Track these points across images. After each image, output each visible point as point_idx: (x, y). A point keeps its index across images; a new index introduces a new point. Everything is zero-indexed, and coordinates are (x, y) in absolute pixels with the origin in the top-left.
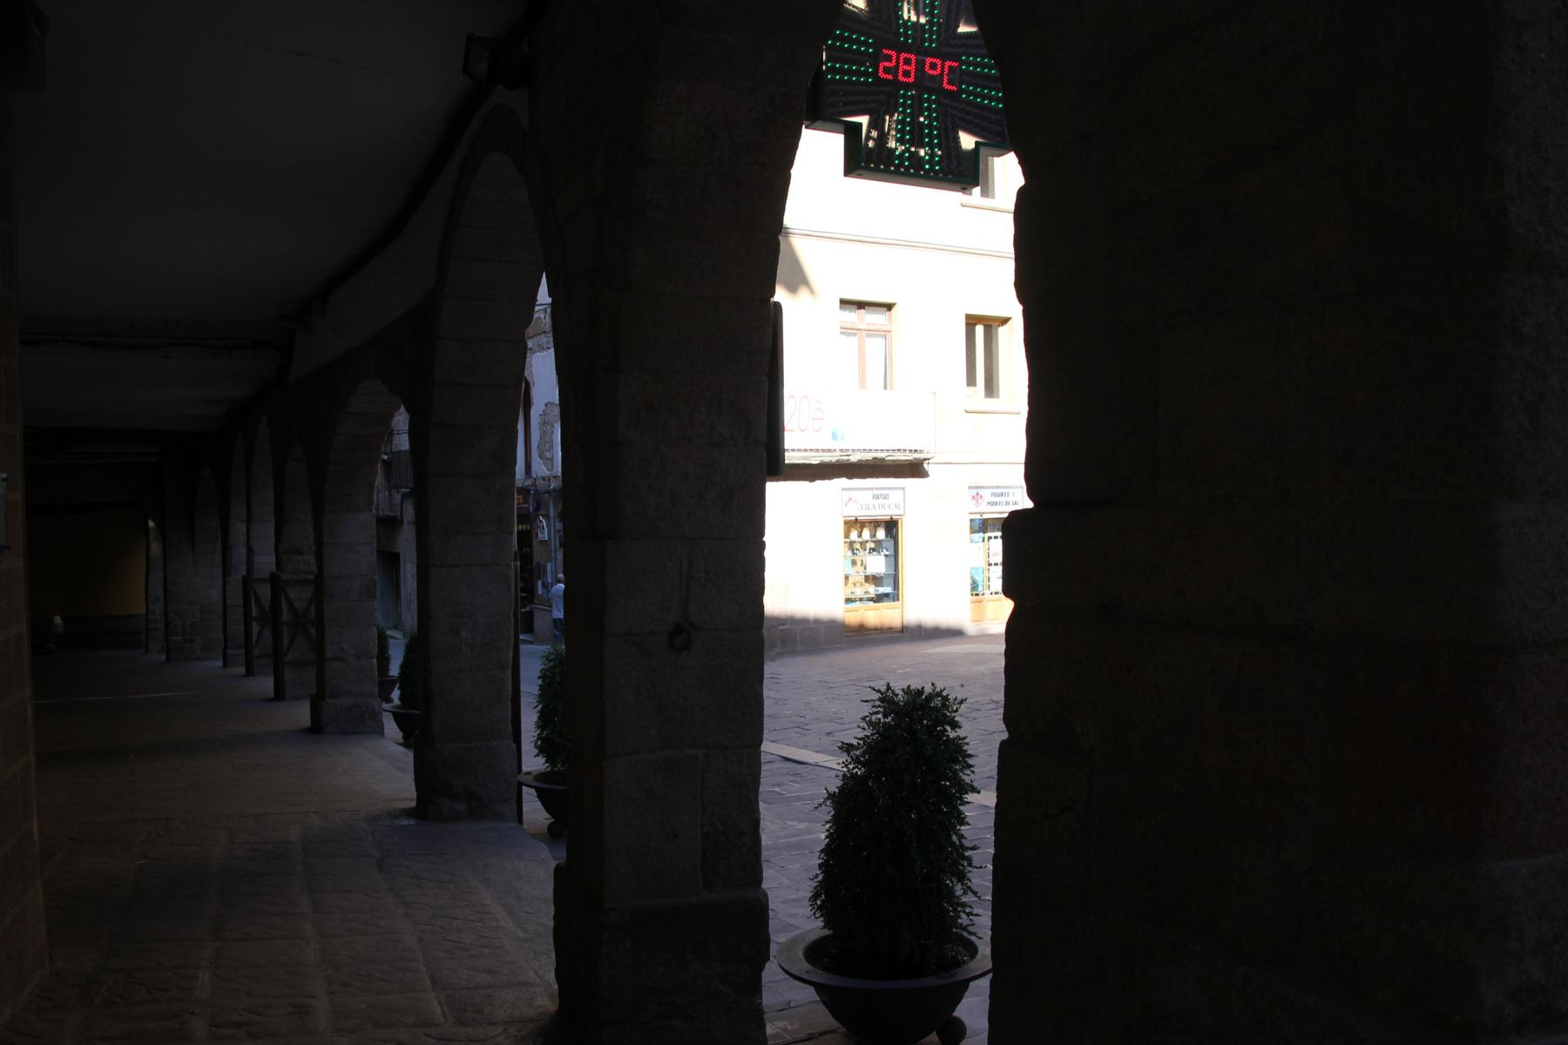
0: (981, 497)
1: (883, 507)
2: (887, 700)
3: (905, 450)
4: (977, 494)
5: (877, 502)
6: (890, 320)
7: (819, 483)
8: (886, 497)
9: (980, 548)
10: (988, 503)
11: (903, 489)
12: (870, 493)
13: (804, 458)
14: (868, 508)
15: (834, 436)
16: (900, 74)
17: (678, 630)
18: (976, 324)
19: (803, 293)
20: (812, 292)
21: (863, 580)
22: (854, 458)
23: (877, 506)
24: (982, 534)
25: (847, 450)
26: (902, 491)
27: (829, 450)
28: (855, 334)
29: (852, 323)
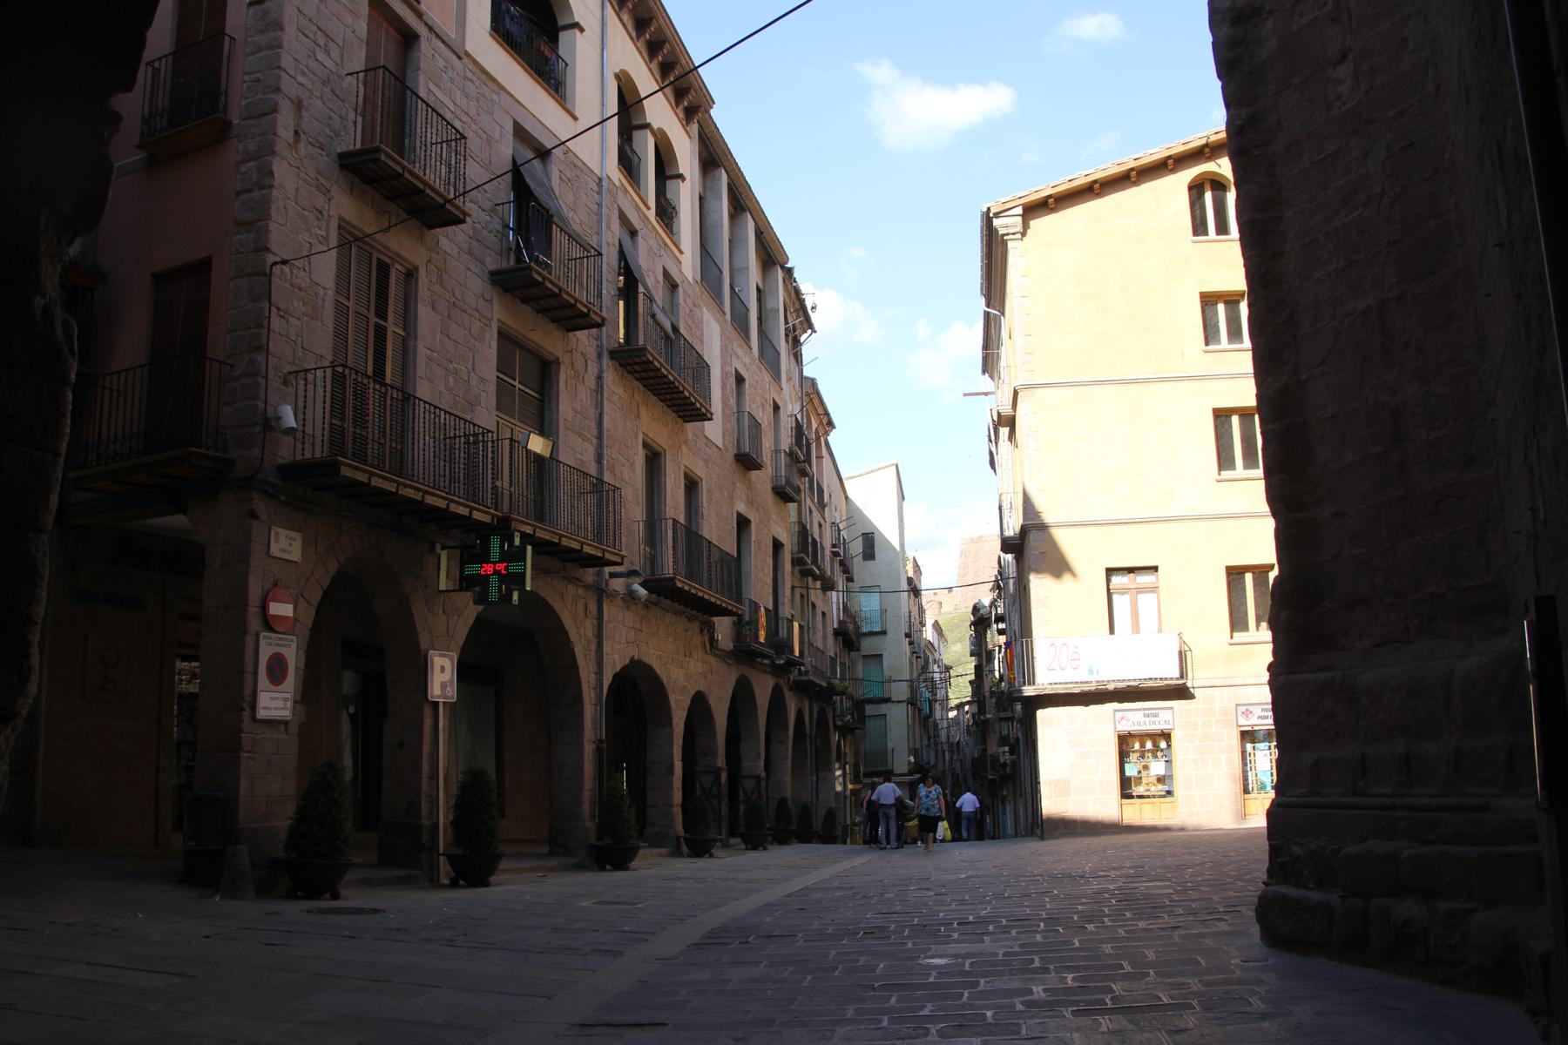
0: (1251, 712)
1: (1154, 723)
2: (626, 869)
3: (1156, 679)
4: (1247, 710)
5: (1147, 720)
6: (1157, 578)
7: (1092, 707)
8: (1156, 715)
9: (1266, 755)
10: (1259, 717)
11: (1171, 708)
12: (1142, 713)
13: (1066, 689)
14: (1139, 724)
15: (1091, 672)
16: (296, 640)
18: (1244, 573)
19: (1067, 578)
20: (1074, 574)
21: (1156, 782)
22: (1111, 687)
23: (1148, 723)
24: (1268, 744)
25: (1103, 681)
26: (1170, 710)
27: (1086, 682)
28: (1127, 593)
29: (1153, 583)
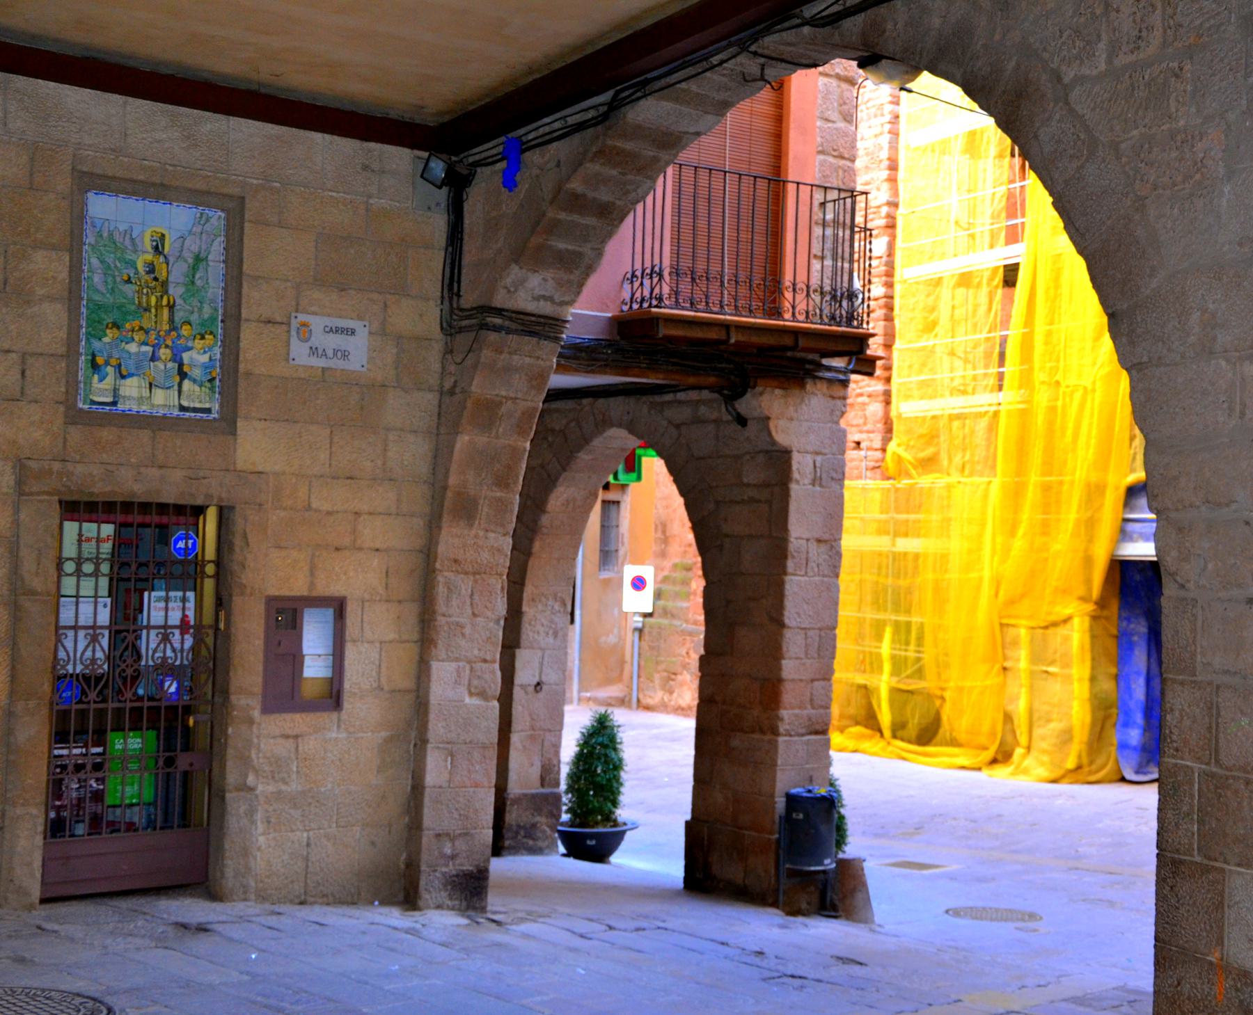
17: (538, 684)
